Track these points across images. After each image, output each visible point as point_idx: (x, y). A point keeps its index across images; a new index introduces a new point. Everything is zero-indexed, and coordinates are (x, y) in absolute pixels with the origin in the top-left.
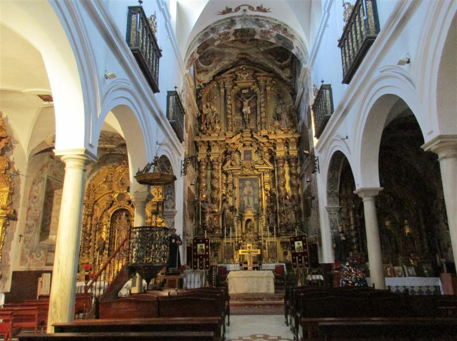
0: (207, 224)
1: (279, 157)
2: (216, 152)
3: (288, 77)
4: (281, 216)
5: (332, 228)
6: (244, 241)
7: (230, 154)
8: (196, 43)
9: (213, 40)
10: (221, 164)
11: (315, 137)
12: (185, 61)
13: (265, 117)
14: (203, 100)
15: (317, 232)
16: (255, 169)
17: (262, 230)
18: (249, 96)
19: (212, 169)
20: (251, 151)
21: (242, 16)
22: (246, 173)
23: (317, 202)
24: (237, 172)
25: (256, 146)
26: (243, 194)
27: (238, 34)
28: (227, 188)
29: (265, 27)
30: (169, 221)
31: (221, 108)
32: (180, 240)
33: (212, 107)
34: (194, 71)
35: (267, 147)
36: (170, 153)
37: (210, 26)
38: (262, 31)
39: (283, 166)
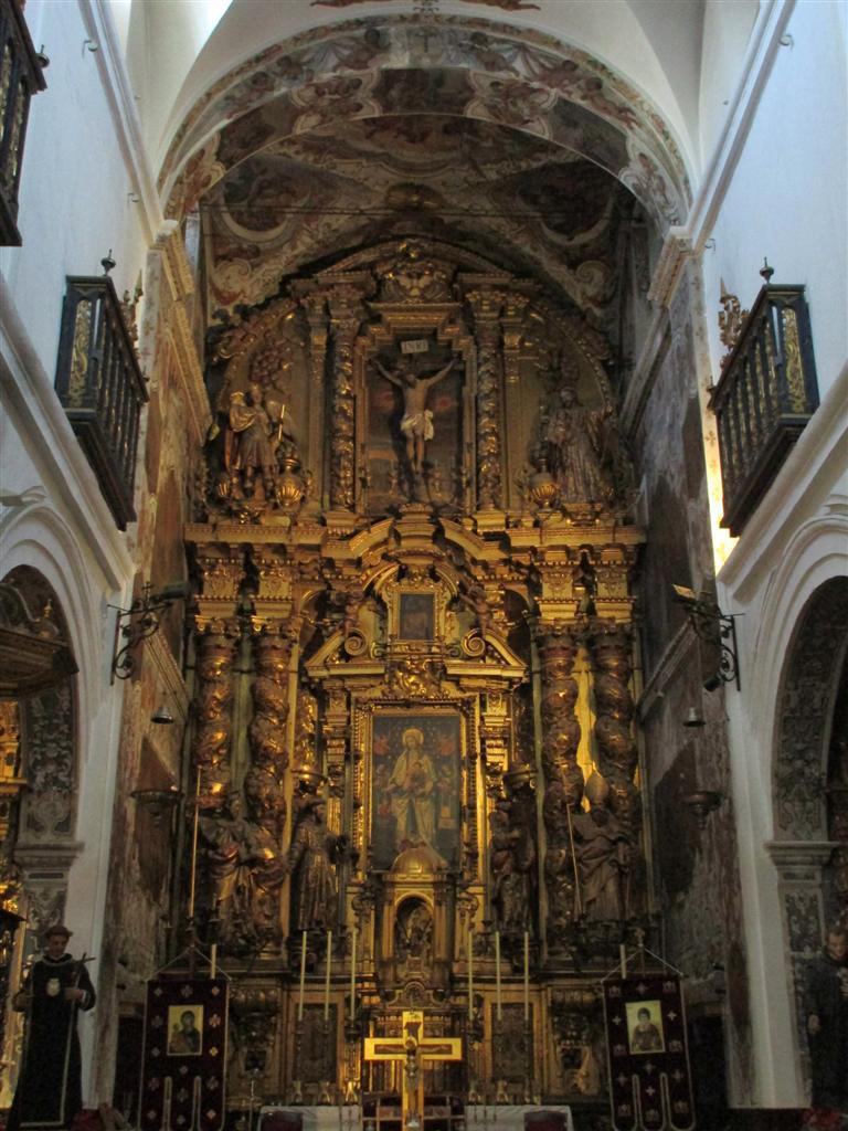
0: (223, 916)
1: (548, 627)
2: (280, 597)
3: (593, 300)
4: (553, 887)
5: (796, 944)
6: (387, 997)
7: (341, 610)
8: (217, 115)
9: (291, 112)
10: (297, 650)
11: (723, 524)
12: (161, 181)
13: (497, 455)
14: (233, 372)
15: (724, 963)
16: (446, 676)
17: (470, 950)
18: (428, 367)
19: (260, 669)
21: (416, 18)
22: (409, 691)
23: (729, 824)
24: (367, 688)
25: (453, 580)
26: (390, 787)
27: (394, 93)
28: (319, 757)
29: (509, 68)
30: (38, 891)
31: (307, 409)
32: (85, 982)
33: (272, 403)
34: (202, 252)
35: (502, 583)
36: (66, 569)
37: (277, 48)
38: (495, 84)
39: (568, 668)
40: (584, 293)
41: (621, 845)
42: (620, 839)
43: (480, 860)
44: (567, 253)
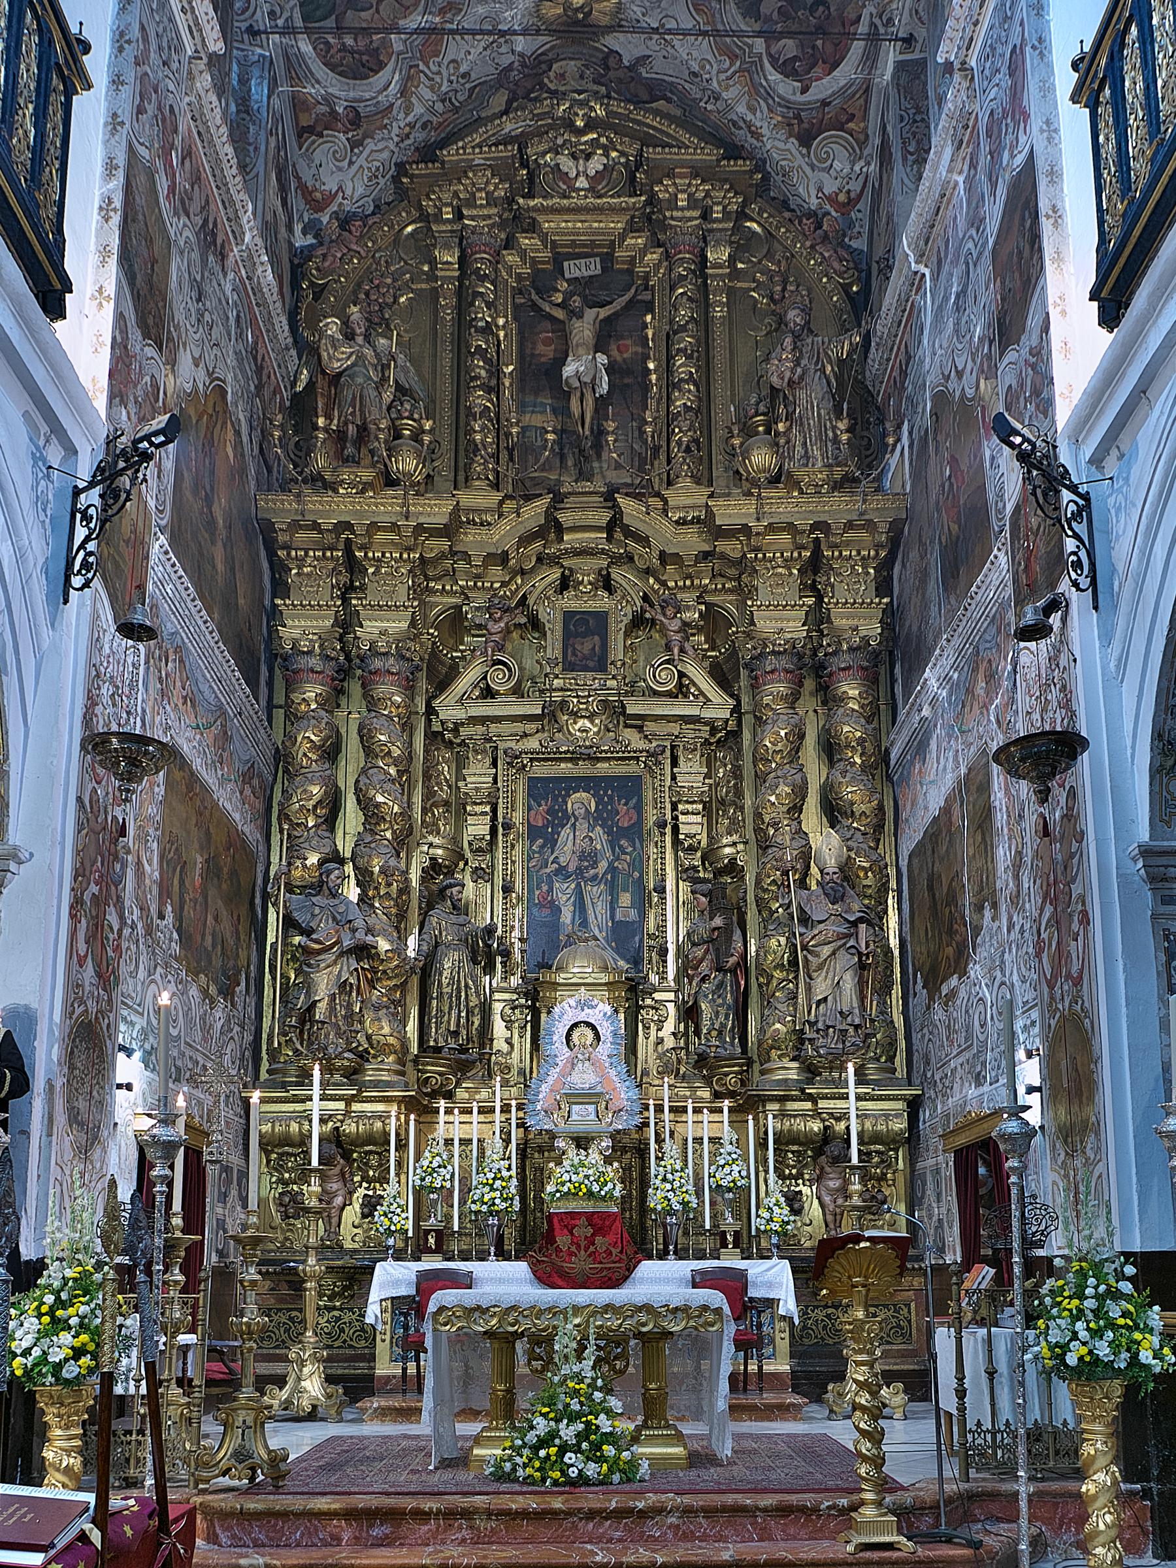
3: (833, 199)
20: (601, 618)
40: (820, 189)
41: (863, 927)
42: (860, 920)
43: (671, 957)
44: (798, 117)
